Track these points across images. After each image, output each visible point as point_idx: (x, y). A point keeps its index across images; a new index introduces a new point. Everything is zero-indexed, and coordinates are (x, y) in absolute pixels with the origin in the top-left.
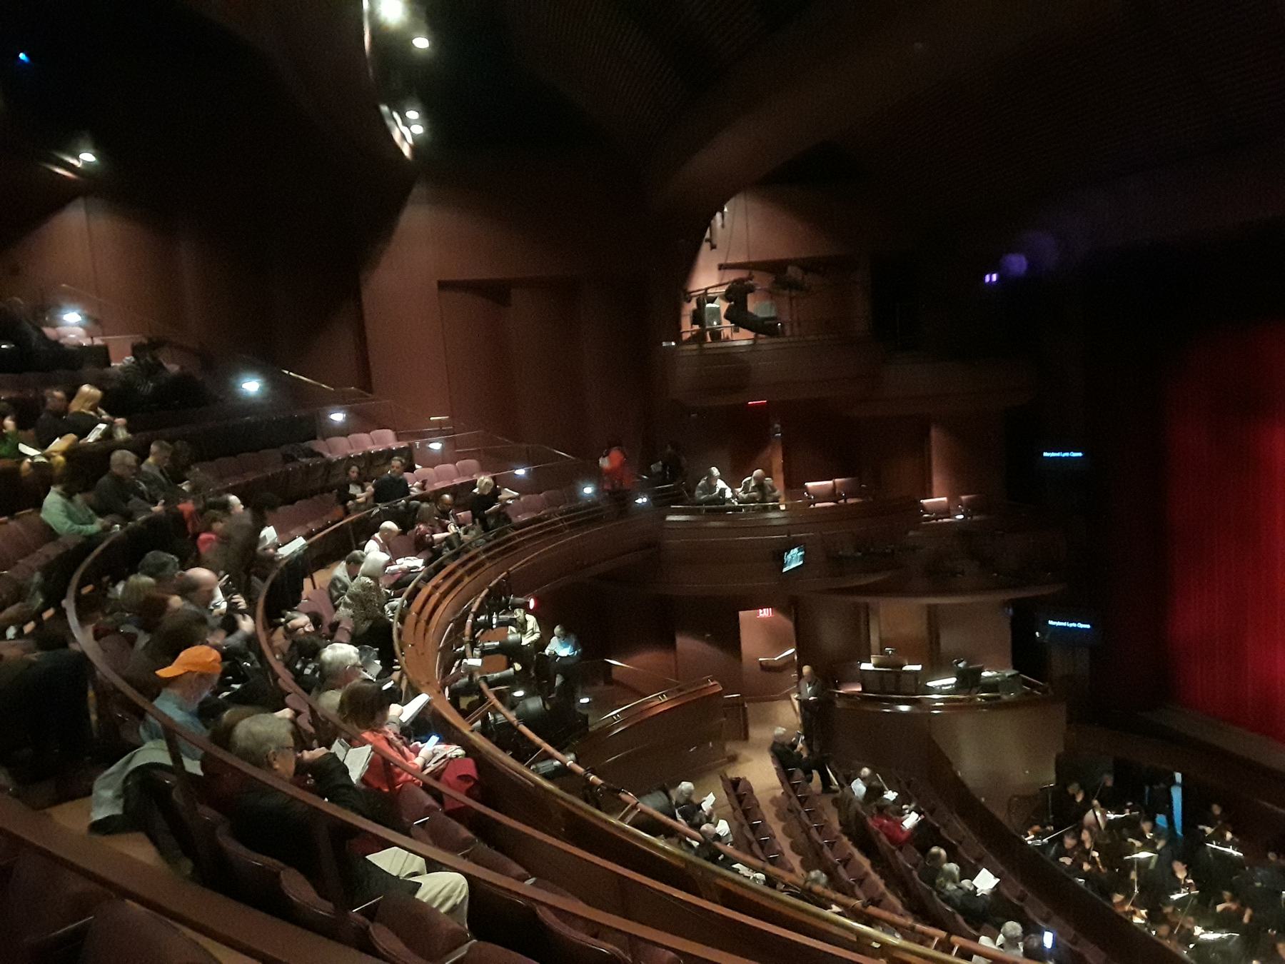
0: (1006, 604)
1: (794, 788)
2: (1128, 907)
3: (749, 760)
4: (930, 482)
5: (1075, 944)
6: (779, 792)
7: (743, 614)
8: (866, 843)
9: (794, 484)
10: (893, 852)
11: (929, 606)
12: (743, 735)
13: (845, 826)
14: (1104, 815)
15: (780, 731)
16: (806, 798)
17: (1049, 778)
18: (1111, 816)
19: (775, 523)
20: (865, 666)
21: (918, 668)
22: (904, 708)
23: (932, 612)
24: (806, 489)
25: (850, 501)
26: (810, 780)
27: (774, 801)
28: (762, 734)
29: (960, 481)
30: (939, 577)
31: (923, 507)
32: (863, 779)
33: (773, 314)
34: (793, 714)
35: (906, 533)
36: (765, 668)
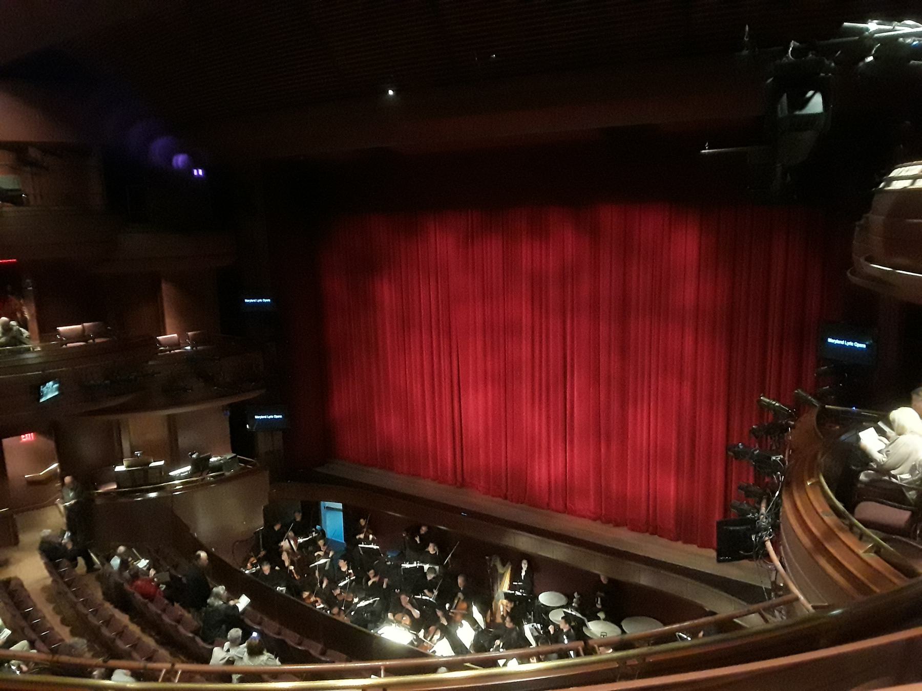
0: (224, 408)
1: (62, 576)
2: (313, 599)
3: (20, 561)
4: (163, 321)
5: (279, 634)
6: (49, 581)
7: (6, 442)
8: (123, 602)
9: (46, 330)
10: (146, 604)
11: (168, 415)
12: (14, 541)
13: (107, 597)
14: (296, 542)
15: (47, 532)
16: (72, 581)
17: (259, 524)
18: (301, 540)
19: (30, 362)
20: (119, 468)
21: (162, 463)
22: (153, 495)
23: (171, 420)
24: (58, 333)
25: (97, 340)
26: (76, 565)
27: (45, 589)
28: (31, 538)
29: (187, 321)
30: (174, 394)
31: (158, 341)
32: (120, 555)
33: (17, 187)
34: (59, 516)
35: (147, 362)
36: (32, 483)
